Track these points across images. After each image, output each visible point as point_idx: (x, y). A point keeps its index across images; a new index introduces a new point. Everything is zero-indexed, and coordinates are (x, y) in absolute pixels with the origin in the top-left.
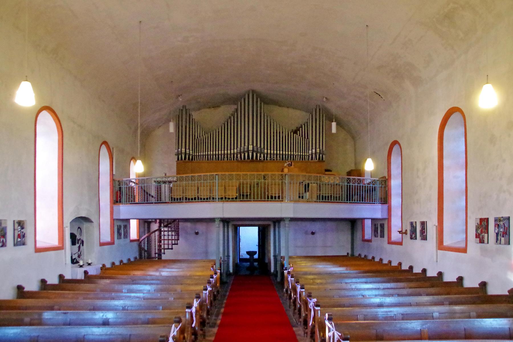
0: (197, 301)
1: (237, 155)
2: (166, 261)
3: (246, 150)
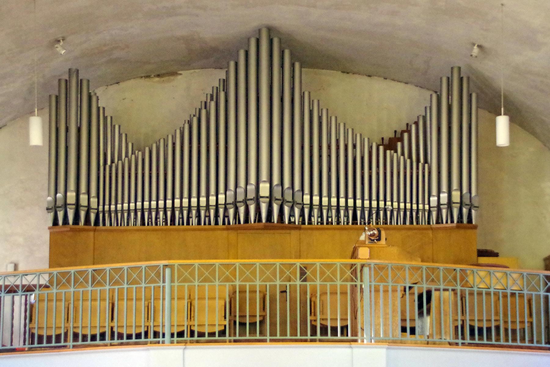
1: (226, 210)
3: (251, 195)
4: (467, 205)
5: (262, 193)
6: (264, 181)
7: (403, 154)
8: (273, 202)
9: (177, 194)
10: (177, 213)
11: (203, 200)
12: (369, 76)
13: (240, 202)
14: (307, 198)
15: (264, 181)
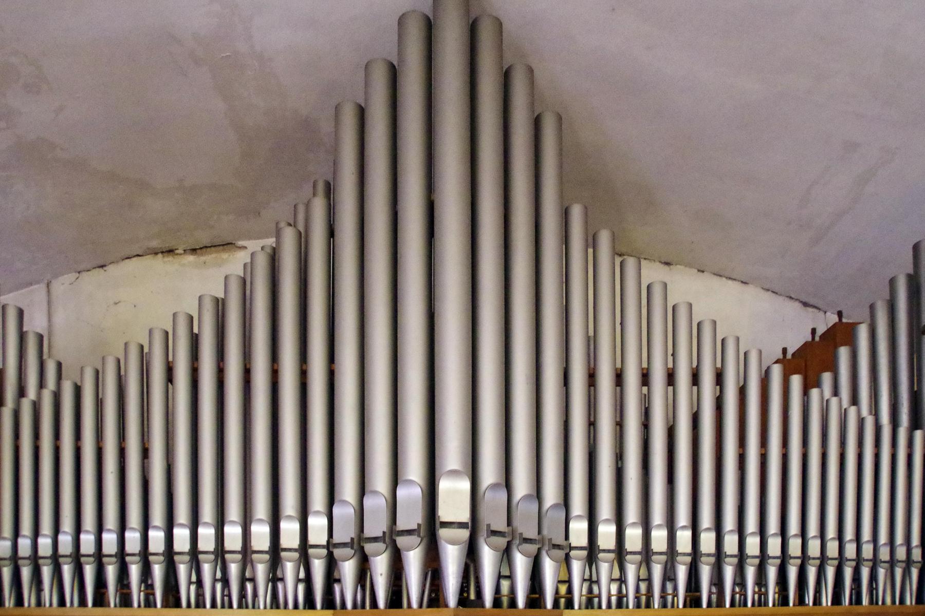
0: (493, 548)
1: (331, 564)
2: (614, 259)
3: (411, 516)
4: (495, 533)
5: (445, 513)
6: (454, 473)
7: (855, 401)
8: (544, 553)
9: (182, 513)
10: (182, 570)
11: (182, 535)
12: (667, 264)
13: (375, 539)
14: (579, 530)
15: (454, 473)
